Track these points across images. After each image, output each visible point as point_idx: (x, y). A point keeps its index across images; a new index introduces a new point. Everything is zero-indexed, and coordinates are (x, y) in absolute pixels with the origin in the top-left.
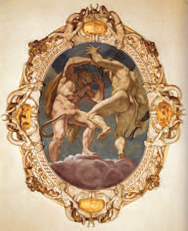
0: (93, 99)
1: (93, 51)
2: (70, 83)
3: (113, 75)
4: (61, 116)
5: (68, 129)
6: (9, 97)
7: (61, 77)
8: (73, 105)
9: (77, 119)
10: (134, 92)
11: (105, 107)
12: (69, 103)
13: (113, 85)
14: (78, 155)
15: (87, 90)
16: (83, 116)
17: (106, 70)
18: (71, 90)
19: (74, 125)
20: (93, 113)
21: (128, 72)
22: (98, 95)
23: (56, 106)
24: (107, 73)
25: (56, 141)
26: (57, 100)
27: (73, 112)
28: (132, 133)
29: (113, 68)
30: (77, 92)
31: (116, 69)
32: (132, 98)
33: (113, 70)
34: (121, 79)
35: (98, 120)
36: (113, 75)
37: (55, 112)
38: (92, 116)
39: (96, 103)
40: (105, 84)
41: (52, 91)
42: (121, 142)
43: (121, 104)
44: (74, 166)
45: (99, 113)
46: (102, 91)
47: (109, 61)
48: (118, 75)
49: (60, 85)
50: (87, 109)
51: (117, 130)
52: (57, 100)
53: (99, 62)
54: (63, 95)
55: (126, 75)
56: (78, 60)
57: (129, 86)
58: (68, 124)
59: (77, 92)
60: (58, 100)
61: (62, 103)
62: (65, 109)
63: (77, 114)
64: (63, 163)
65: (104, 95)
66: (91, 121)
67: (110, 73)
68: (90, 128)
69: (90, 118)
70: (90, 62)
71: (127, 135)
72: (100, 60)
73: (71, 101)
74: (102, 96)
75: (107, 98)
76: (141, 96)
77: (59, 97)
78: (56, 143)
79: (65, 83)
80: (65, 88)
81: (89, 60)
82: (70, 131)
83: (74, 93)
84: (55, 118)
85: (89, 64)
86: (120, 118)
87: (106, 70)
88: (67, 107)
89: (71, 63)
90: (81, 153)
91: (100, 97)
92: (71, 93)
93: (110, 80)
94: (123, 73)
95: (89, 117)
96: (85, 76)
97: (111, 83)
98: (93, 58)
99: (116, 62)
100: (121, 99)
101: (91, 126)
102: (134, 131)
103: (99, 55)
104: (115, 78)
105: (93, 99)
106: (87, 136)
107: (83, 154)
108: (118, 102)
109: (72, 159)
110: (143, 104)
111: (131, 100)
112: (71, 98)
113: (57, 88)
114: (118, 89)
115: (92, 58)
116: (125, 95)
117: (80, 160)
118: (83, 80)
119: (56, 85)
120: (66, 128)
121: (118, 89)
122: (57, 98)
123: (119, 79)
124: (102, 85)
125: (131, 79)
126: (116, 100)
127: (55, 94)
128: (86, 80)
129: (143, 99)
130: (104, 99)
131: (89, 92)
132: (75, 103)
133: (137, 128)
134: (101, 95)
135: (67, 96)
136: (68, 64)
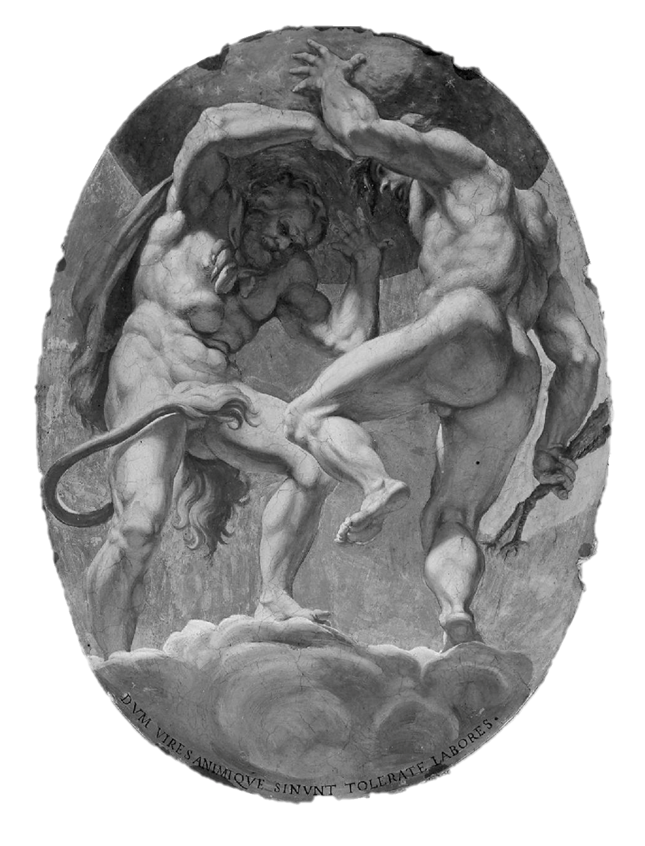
0: (319, 330)
1: (330, 78)
2: (203, 246)
3: (429, 205)
4: (150, 418)
5: (186, 484)
6: (422, 519)
7: (157, 208)
8: (215, 357)
9: (232, 435)
10: (533, 303)
11: (386, 373)
12: (193, 346)
13: (426, 257)
14: (237, 621)
15: (292, 284)
16: (271, 421)
17: (391, 180)
18: (208, 278)
19: (212, 463)
20: (321, 403)
21: (504, 194)
22: (347, 316)
23: (131, 360)
24: (401, 196)
25: (123, 542)
26: (133, 330)
27: (215, 395)
28: (514, 516)
29: (428, 171)
30: (236, 290)
31: (442, 175)
32: (526, 328)
33: (427, 182)
34: (467, 238)
35: (340, 436)
36: (429, 205)
37: (123, 394)
38: (309, 418)
39: (334, 353)
40: (382, 250)
41: (109, 283)
42: (451, 560)
43: (462, 365)
44: (214, 682)
45: (347, 403)
46: (369, 287)
47: (412, 134)
48: (450, 201)
49: (150, 250)
50: (286, 385)
51: (442, 500)
52: (133, 330)
53: (354, 134)
54: (164, 305)
55: (497, 211)
56: (242, 120)
57: (514, 261)
58: (190, 460)
59: (236, 290)
60: (141, 332)
61: (158, 348)
62: (175, 380)
63: (236, 410)
64: (155, 661)
65: (377, 312)
66: (305, 445)
67: (415, 197)
68: (298, 484)
69: (299, 434)
70: (312, 132)
71: (490, 526)
72: (364, 126)
73: (205, 337)
74: (370, 315)
75: (392, 327)
76: (569, 325)
77: (146, 314)
78: (123, 555)
79: (176, 240)
80: (182, 268)
81: (306, 122)
82: (197, 496)
83: (222, 295)
84: (122, 424)
85: (304, 144)
86: (457, 433)
87: (395, 176)
88: (183, 369)
89: (215, 135)
90: (251, 613)
91: (356, 325)
92: (205, 297)
93: (409, 233)
94: (475, 202)
95: (294, 426)
96: (282, 206)
97: (416, 246)
98: (329, 114)
99: (446, 139)
100: (466, 335)
101: (308, 469)
102: (527, 505)
103: (360, 100)
104: (435, 220)
105: (319, 330)
106: (285, 520)
107: (263, 617)
108: (265, 785)
109: (205, 639)
110: (579, 366)
111: (521, 340)
112: (207, 321)
113: (134, 264)
114: (459, 274)
115: (320, 115)
116: (490, 316)
117: (246, 647)
118: (274, 231)
119: (134, 245)
120: (178, 479)
121: (459, 274)
122: (133, 320)
123: (459, 231)
124: (370, 258)
125: (521, 231)
126: (440, 342)
127: (124, 298)
128: (284, 231)
129: (579, 340)
130: (375, 333)
131: (299, 297)
132: (229, 352)
133: (539, 492)
134: (361, 312)
135: (187, 314)
136: (196, 139)
